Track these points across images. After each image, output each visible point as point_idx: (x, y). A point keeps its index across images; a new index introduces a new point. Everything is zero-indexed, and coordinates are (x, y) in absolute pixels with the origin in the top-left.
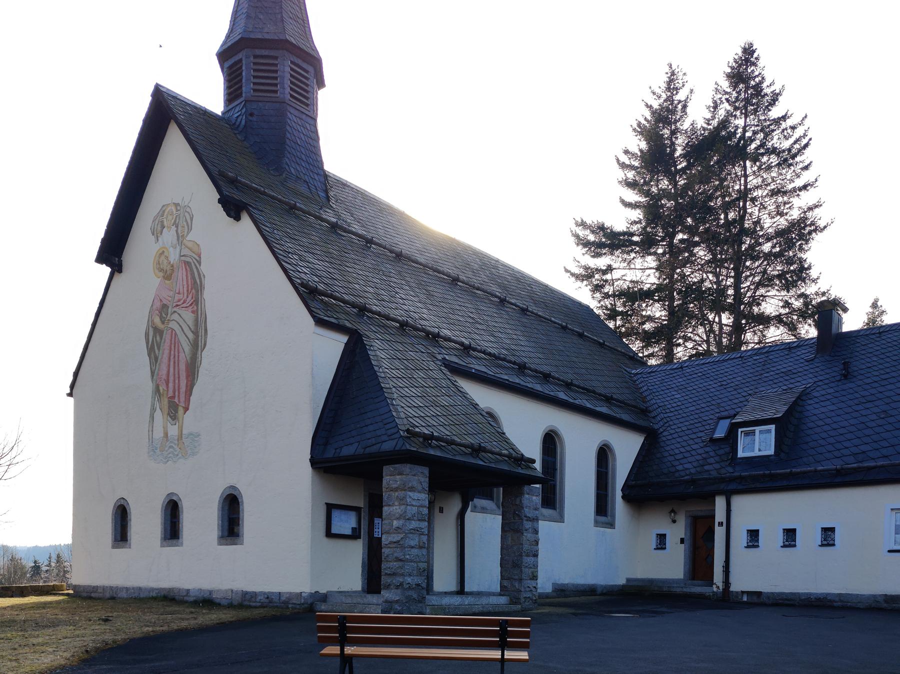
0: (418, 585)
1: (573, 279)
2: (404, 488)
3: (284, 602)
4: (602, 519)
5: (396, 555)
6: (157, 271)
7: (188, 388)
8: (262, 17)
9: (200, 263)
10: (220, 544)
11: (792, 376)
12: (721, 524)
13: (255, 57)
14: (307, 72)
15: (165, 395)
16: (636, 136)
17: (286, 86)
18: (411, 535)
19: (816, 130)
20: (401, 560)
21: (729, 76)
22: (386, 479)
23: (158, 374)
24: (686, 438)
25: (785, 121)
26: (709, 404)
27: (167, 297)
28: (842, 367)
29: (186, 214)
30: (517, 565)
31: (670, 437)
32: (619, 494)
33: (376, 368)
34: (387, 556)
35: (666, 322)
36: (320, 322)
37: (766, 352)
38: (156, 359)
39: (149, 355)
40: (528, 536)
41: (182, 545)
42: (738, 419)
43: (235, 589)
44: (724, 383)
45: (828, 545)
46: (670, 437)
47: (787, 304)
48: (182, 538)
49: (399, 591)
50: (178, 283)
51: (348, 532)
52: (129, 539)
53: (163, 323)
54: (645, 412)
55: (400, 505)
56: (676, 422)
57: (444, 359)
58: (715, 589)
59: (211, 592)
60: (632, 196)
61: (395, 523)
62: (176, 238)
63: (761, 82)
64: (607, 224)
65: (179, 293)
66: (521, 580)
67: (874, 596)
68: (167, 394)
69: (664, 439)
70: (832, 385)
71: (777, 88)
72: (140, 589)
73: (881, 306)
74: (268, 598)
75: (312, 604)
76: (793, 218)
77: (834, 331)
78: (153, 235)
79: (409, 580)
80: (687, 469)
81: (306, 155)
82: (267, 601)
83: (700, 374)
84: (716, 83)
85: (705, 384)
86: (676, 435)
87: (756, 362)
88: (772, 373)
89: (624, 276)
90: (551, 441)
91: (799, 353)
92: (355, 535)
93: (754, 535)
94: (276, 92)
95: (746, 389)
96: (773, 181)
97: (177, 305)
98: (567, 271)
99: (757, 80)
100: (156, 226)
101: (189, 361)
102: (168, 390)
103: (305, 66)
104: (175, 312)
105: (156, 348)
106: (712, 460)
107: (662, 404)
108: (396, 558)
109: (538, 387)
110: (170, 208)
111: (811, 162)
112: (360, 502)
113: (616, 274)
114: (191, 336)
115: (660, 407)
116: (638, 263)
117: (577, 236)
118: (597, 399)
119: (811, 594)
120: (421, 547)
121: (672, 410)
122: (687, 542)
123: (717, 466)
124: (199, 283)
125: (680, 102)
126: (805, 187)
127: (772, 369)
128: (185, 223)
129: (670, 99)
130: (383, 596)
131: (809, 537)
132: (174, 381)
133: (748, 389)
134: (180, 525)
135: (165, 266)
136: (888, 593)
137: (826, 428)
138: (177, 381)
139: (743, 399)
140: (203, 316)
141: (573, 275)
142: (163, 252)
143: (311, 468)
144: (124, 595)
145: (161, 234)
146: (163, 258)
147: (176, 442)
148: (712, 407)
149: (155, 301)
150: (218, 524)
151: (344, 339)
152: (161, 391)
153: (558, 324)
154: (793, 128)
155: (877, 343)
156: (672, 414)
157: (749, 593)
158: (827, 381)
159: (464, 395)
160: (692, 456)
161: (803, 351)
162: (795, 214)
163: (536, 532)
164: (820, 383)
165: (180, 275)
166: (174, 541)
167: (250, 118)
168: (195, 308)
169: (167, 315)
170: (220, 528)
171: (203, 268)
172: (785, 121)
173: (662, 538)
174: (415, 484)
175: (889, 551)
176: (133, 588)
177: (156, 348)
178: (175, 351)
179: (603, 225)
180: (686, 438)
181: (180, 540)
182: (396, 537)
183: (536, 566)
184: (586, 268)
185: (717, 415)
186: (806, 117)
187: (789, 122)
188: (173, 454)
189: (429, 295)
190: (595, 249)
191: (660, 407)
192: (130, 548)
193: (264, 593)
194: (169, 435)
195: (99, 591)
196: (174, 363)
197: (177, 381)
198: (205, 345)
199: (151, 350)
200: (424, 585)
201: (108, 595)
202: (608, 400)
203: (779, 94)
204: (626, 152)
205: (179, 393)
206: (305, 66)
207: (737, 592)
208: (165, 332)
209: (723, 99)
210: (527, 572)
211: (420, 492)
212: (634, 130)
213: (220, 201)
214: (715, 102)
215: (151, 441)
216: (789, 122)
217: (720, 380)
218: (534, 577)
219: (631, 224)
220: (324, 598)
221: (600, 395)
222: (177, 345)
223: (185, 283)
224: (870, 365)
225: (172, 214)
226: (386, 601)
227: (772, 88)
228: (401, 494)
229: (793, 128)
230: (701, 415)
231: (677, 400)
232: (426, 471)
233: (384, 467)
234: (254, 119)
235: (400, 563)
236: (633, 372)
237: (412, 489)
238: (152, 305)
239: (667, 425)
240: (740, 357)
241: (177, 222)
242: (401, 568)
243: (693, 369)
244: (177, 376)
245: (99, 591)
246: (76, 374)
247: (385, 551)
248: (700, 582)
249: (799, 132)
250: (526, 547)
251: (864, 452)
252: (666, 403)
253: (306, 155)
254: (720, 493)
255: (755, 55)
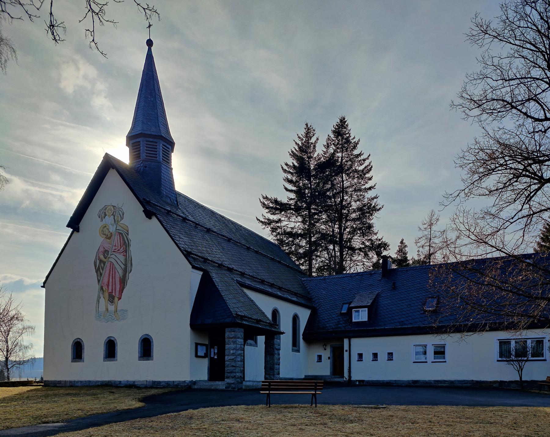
0: (241, 376)
1: (261, 224)
2: (235, 337)
3: (176, 385)
4: (295, 348)
5: (232, 364)
6: (101, 234)
7: (121, 289)
8: (149, 123)
9: (128, 235)
10: (139, 360)
11: (373, 287)
12: (346, 351)
13: (147, 141)
14: (168, 148)
15: (106, 291)
16: (291, 157)
17: (161, 155)
18: (238, 356)
19: (374, 161)
20: (234, 367)
21: (334, 132)
22: (227, 334)
23: (102, 281)
24: (329, 312)
25: (360, 156)
26: (338, 297)
27: (108, 247)
28: (392, 284)
29: (120, 212)
30: (272, 369)
31: (322, 311)
32: (301, 337)
33: (217, 287)
34: (228, 365)
35: (308, 249)
36: (194, 267)
37: (361, 275)
38: (101, 274)
39: (97, 272)
40: (276, 356)
41: (117, 360)
42: (352, 305)
43: (148, 380)
44: (344, 287)
45: (390, 360)
46: (322, 311)
47: (363, 243)
48: (117, 357)
49: (234, 379)
50: (115, 241)
51: (203, 355)
52: (83, 358)
53: (105, 258)
54: (310, 299)
55: (234, 344)
56: (324, 304)
57: (237, 280)
58: (345, 379)
59: (134, 382)
60: (290, 187)
61: (232, 352)
62: (114, 221)
63: (348, 137)
64: (279, 199)
65: (115, 246)
66: (274, 375)
67: (409, 381)
68: (108, 291)
69: (319, 312)
70: (389, 292)
71: (356, 140)
72: (90, 381)
73: (405, 243)
74: (167, 384)
75: (190, 386)
76: (365, 202)
77: (388, 268)
78: (99, 217)
79: (238, 374)
80: (331, 326)
81: (169, 186)
82: (166, 385)
83: (333, 283)
84: (328, 136)
85: (336, 287)
86: (324, 311)
87: (357, 279)
88: (364, 285)
89: (287, 225)
90: (275, 313)
91: (375, 277)
92: (205, 356)
93: (360, 356)
94: (156, 157)
95: (354, 291)
96: (355, 184)
97: (114, 251)
98: (258, 220)
99: (347, 135)
100: (101, 214)
101: (122, 277)
102: (108, 289)
103: (168, 146)
104: (112, 254)
105: (101, 269)
106: (341, 323)
107: (317, 296)
108: (232, 365)
109: (270, 290)
110: (110, 207)
111: (372, 176)
112: (207, 342)
113: (284, 224)
114: (123, 266)
115: (316, 297)
116: (293, 219)
117: (264, 204)
118: (292, 294)
119: (384, 380)
120: (241, 361)
121: (322, 298)
122: (331, 358)
123: (344, 325)
124: (127, 243)
125: (312, 143)
126: (370, 188)
127: (364, 283)
128: (119, 216)
129: (307, 142)
130: (226, 381)
131: (383, 357)
132: (112, 285)
133: (354, 291)
134: (116, 352)
135: (107, 232)
136: (414, 379)
137: (388, 310)
138: (114, 286)
139: (352, 296)
140: (130, 258)
141: (262, 222)
142: (106, 226)
143: (190, 328)
144: (79, 384)
145: (104, 218)
146: (105, 229)
147: (114, 313)
148: (340, 298)
149: (100, 248)
150: (139, 351)
151: (201, 273)
152: (104, 289)
153: (270, 257)
154: (364, 160)
155: (406, 275)
156: (322, 301)
157: (359, 381)
158: (387, 290)
159: (247, 296)
160: (333, 320)
161: (377, 276)
162: (366, 200)
163: (279, 355)
164: (384, 291)
165: (116, 238)
166: (112, 359)
167: (145, 168)
168: (125, 254)
169: (108, 255)
170: (140, 353)
171: (130, 237)
172: (360, 156)
173: (320, 358)
174: (240, 336)
175: (414, 362)
176: (85, 381)
177: (101, 269)
178: (113, 271)
179: (277, 200)
180: (329, 312)
181: (116, 358)
182: (232, 357)
183: (279, 369)
184: (268, 220)
185: (343, 302)
186: (370, 155)
187: (362, 157)
188: (112, 319)
189: (223, 249)
190: (272, 210)
191: (316, 297)
192: (83, 362)
193: (165, 382)
194: (109, 310)
195: (62, 383)
196: (112, 277)
197: (114, 286)
198: (131, 271)
199: (97, 270)
200: (242, 377)
201: (68, 385)
202: (295, 294)
203: (357, 143)
204: (287, 165)
205: (115, 291)
206: (168, 146)
207: (354, 381)
208: (106, 263)
209: (332, 143)
210: (276, 371)
211: (241, 339)
212: (290, 154)
213: (143, 211)
214: (328, 144)
215: (97, 312)
216: (362, 157)
217: (342, 286)
218: (279, 374)
219: (290, 200)
220: (194, 383)
221: (293, 292)
222: (114, 269)
223: (119, 242)
224: (403, 284)
225: (111, 210)
226: (228, 383)
227: (354, 140)
228: (234, 340)
229: (364, 160)
230: (335, 302)
231: (323, 294)
232: (243, 330)
233: (226, 329)
234: (147, 169)
235: (234, 368)
236: (302, 279)
237: (239, 338)
238: (98, 250)
239: (320, 305)
240: (350, 276)
241: (114, 214)
242: (235, 369)
243: (330, 280)
244: (114, 283)
245: (62, 383)
246: (47, 277)
247: (227, 363)
248: (338, 376)
249: (367, 163)
250: (276, 361)
251: (403, 321)
252: (319, 295)
253: (169, 186)
254: (346, 338)
255: (346, 124)
